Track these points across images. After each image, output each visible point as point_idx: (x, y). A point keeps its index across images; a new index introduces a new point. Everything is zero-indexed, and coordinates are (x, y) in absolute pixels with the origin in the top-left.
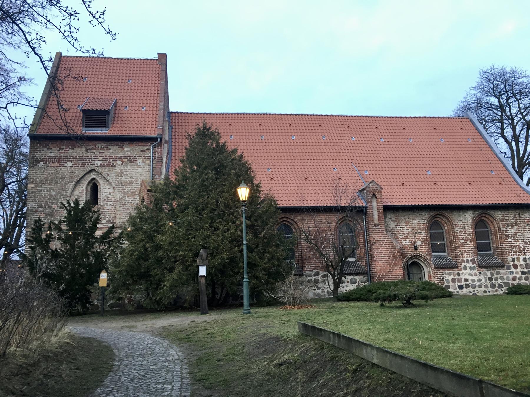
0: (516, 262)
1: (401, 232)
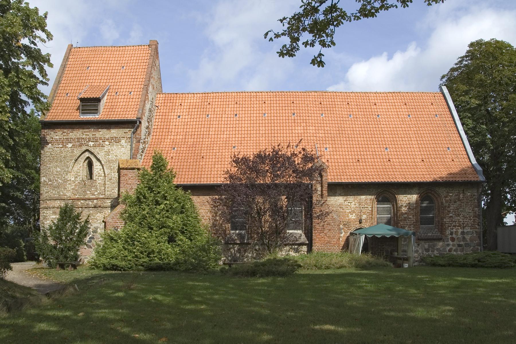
0: (454, 236)
1: (349, 207)
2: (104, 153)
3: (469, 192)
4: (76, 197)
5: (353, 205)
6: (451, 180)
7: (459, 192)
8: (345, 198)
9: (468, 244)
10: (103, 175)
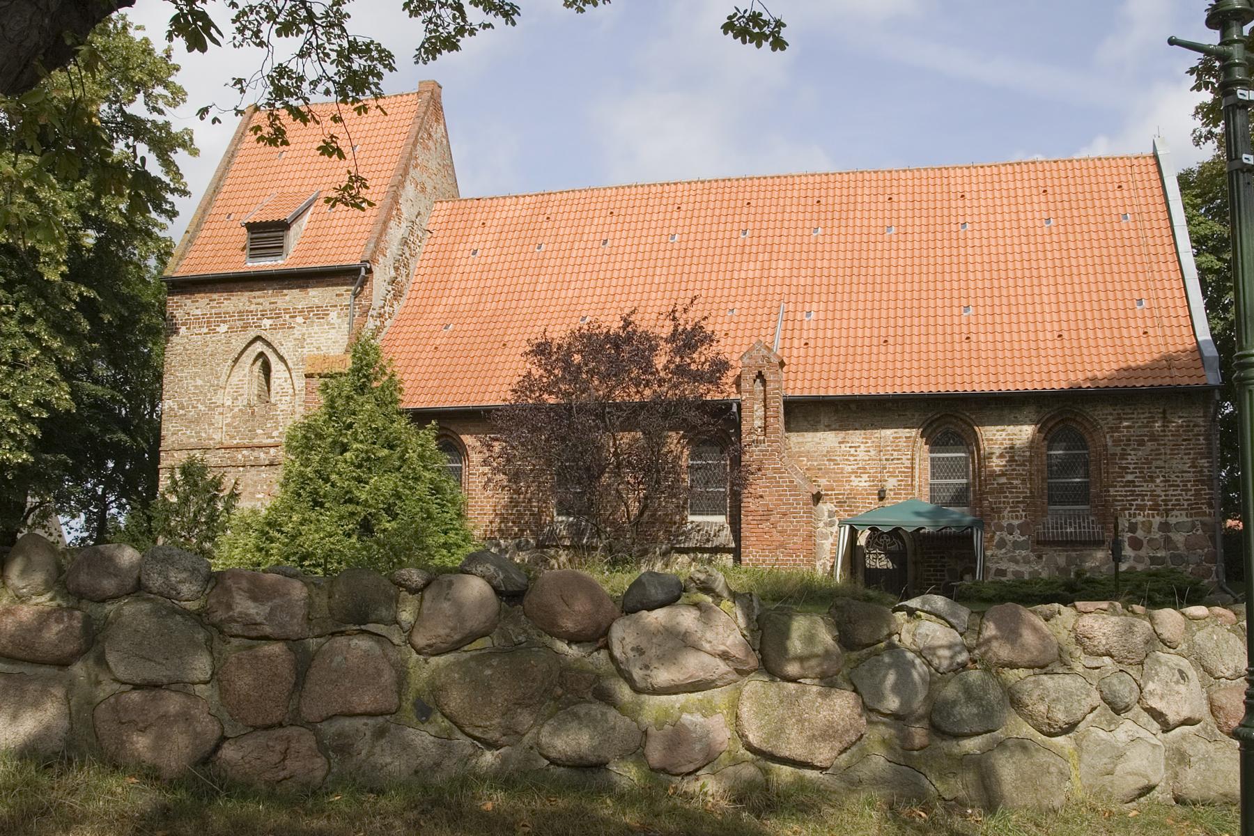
0: (1140, 534)
1: (852, 458)
2: (293, 343)
3: (1180, 417)
4: (235, 442)
5: (861, 454)
6: (1121, 384)
7: (1153, 417)
8: (842, 434)
9: (1180, 556)
10: (291, 391)
